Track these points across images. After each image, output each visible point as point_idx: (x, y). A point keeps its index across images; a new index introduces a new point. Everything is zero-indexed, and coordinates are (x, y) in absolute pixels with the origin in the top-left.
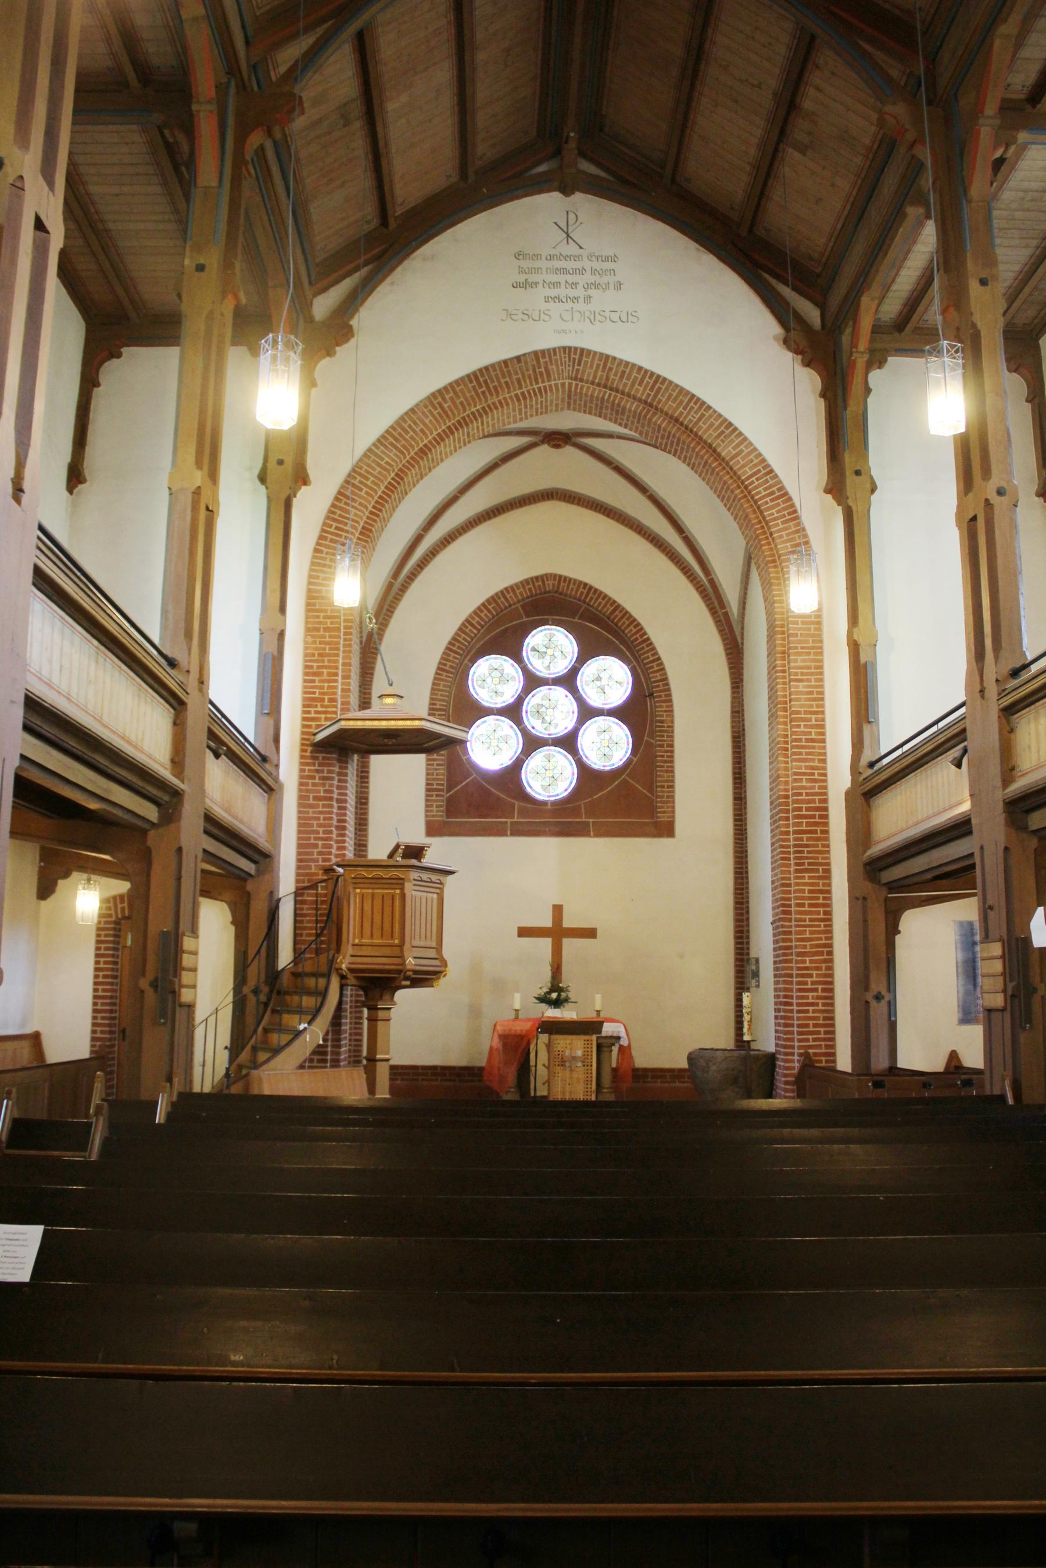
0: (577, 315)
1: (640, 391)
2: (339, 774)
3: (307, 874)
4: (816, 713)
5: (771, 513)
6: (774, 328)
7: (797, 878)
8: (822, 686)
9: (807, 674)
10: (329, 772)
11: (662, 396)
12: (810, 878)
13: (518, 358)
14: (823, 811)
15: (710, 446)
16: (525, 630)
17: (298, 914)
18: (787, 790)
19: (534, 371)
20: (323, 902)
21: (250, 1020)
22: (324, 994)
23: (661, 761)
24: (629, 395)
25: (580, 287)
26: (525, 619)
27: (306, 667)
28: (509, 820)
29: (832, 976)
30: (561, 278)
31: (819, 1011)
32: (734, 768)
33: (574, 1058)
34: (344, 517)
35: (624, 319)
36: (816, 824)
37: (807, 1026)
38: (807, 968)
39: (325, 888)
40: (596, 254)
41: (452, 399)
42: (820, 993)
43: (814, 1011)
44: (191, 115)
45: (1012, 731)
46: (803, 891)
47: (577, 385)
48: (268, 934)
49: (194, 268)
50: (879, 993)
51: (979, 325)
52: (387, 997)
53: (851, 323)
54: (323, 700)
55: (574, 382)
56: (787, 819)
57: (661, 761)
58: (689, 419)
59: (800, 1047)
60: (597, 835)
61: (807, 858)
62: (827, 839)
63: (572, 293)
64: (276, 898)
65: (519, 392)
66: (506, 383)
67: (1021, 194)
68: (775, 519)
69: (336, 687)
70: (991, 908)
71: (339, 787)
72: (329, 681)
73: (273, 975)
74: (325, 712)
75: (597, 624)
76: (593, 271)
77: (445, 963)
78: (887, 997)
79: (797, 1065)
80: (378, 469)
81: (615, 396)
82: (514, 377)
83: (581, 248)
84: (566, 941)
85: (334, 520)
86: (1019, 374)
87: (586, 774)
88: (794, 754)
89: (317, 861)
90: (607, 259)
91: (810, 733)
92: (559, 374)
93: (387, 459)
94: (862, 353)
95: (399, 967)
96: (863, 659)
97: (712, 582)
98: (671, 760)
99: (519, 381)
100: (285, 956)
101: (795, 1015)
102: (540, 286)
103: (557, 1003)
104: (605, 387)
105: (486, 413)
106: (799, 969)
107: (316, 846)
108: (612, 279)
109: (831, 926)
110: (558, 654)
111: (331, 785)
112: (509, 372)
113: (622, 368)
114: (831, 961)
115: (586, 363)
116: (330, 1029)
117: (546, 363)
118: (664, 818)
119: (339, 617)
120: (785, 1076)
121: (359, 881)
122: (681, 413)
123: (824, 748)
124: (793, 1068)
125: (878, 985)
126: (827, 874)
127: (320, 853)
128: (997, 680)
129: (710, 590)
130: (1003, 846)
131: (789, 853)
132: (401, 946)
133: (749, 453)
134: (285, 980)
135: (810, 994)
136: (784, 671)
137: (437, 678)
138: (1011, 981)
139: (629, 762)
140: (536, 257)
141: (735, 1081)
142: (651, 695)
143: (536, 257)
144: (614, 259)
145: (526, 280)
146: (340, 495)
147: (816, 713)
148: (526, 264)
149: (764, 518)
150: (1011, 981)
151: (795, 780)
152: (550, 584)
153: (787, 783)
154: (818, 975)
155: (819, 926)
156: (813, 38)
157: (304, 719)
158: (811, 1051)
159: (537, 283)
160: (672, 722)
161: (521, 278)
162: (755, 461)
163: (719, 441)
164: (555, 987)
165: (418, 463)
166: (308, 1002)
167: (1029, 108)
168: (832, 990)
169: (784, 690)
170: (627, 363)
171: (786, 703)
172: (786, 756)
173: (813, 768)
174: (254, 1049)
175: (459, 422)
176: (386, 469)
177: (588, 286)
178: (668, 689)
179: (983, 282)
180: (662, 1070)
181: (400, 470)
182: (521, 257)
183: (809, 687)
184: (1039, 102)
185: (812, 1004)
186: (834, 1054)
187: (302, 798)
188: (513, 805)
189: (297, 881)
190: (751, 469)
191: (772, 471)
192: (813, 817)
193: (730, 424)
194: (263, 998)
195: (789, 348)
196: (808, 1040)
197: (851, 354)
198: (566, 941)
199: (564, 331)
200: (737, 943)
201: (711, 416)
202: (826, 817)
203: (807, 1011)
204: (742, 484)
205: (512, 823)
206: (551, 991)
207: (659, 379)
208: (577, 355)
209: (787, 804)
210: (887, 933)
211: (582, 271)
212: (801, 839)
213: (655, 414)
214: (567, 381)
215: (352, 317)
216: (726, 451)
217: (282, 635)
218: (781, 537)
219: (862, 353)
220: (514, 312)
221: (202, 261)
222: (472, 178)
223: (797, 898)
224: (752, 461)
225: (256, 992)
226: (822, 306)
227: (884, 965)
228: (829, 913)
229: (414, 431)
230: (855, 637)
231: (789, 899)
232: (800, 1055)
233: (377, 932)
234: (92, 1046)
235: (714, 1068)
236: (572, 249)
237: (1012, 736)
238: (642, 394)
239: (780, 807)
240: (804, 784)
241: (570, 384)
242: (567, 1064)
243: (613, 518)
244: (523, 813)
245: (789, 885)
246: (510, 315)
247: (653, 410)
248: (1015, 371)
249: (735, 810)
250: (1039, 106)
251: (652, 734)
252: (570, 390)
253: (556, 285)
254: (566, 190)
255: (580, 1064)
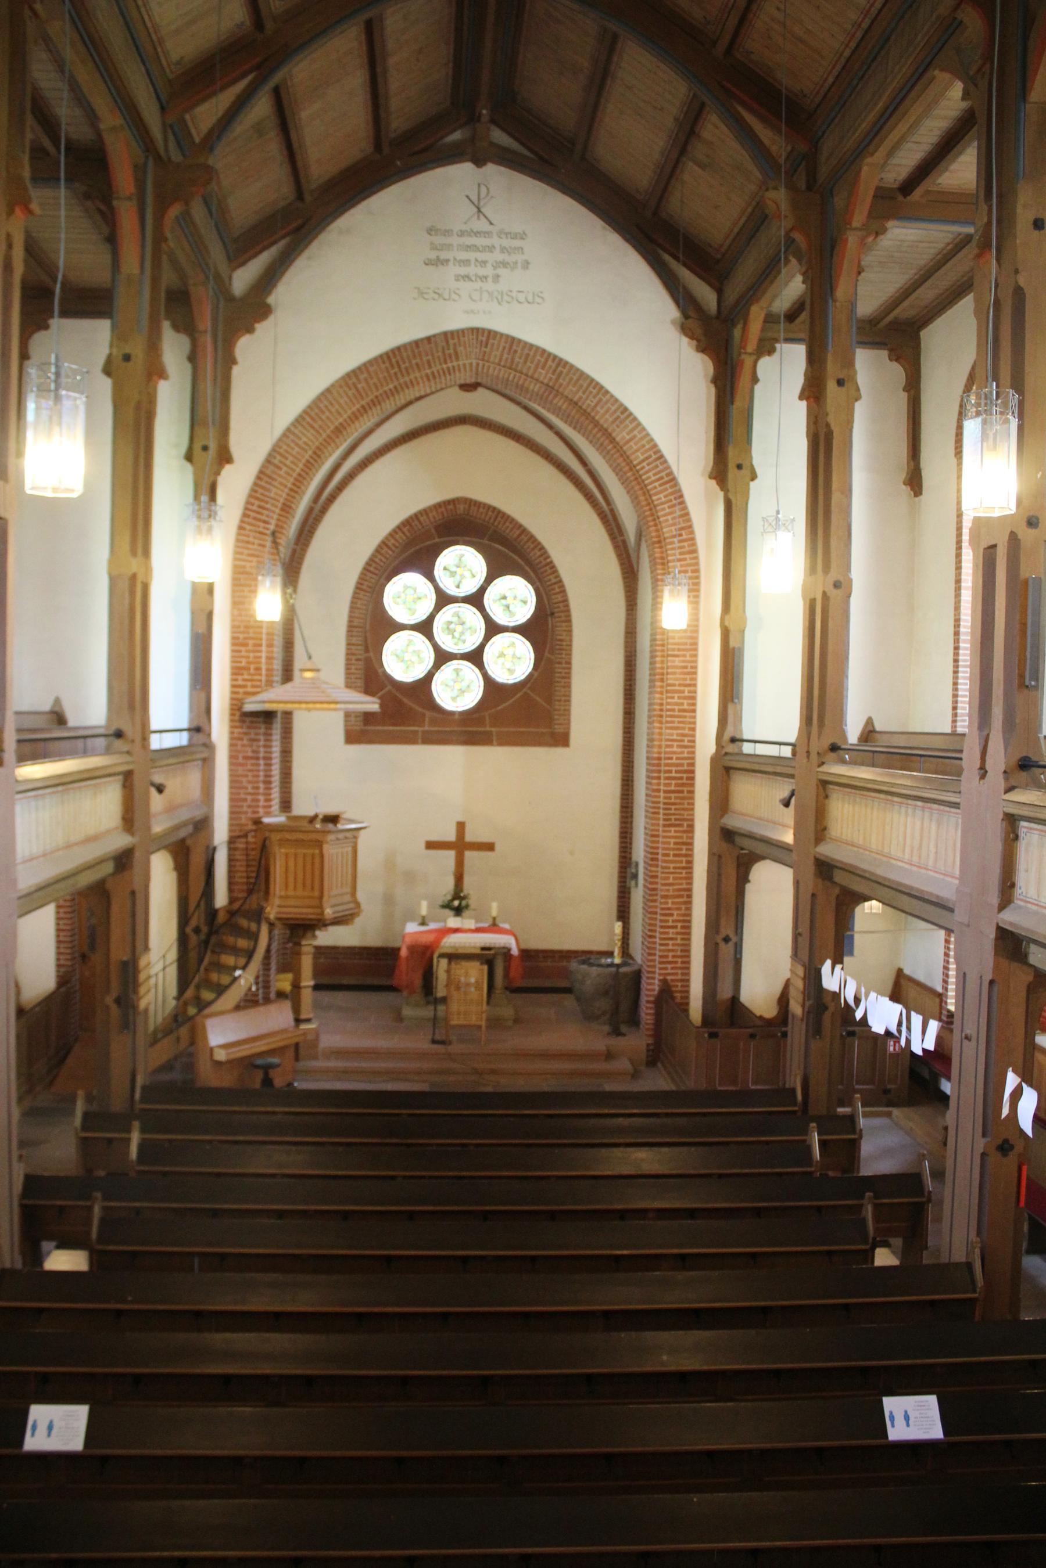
0: (485, 295)
1: (542, 374)
2: (265, 734)
3: (238, 825)
4: (689, 685)
5: (659, 498)
6: (672, 311)
7: (664, 831)
8: (696, 662)
9: (684, 650)
10: (257, 734)
11: (564, 380)
12: (676, 831)
13: (428, 339)
14: (691, 773)
15: (606, 430)
16: (435, 552)
17: (231, 860)
18: (660, 753)
19: (443, 352)
20: (252, 872)
21: (193, 955)
22: (255, 937)
23: (559, 677)
24: (532, 377)
25: (489, 265)
26: (437, 540)
27: (233, 638)
28: (420, 729)
29: (690, 915)
30: (472, 256)
31: (678, 945)
32: (625, 685)
33: (468, 985)
34: (266, 496)
35: (530, 299)
36: (683, 785)
37: (667, 957)
38: (669, 909)
39: (255, 837)
40: (506, 231)
41: (366, 380)
42: (679, 930)
43: (673, 945)
44: (112, 209)
45: (827, 797)
46: (669, 843)
47: (484, 365)
48: (203, 894)
49: (120, 358)
50: (727, 936)
51: (833, 426)
52: (309, 934)
53: (742, 322)
54: (249, 669)
55: (481, 363)
56: (659, 778)
57: (559, 677)
58: (589, 403)
59: (660, 974)
60: (500, 744)
61: (674, 814)
62: (692, 798)
63: (482, 271)
64: (211, 848)
65: (428, 371)
66: (417, 364)
67: (899, 243)
68: (663, 503)
69: (260, 657)
70: (800, 934)
71: (265, 746)
72: (253, 651)
73: (212, 913)
74: (252, 680)
75: (502, 544)
76: (503, 249)
77: (358, 905)
78: (734, 939)
79: (657, 988)
80: (297, 449)
81: (520, 377)
82: (425, 359)
83: (491, 224)
84: (468, 854)
85: (257, 499)
86: (900, 363)
87: (492, 688)
88: (667, 722)
89: (246, 813)
90: (515, 236)
91: (682, 704)
92: (467, 356)
93: (305, 439)
94: (750, 354)
95: (319, 917)
96: (733, 643)
97: (612, 511)
98: (568, 676)
99: (428, 362)
100: (221, 898)
101: (658, 947)
102: (451, 263)
103: (458, 911)
104: (510, 368)
105: (398, 392)
106: (663, 909)
107: (245, 800)
108: (519, 258)
109: (691, 873)
110: (468, 574)
111: (259, 746)
112: (420, 352)
113: (526, 351)
114: (690, 903)
115: (493, 345)
116: (261, 973)
117: (455, 345)
118: (559, 729)
119: (261, 627)
120: (647, 996)
121: (283, 842)
122: (581, 398)
123: (694, 717)
124: (653, 990)
125: (727, 930)
126: (691, 828)
127: (249, 806)
128: (818, 753)
129: (610, 517)
130: (811, 892)
131: (659, 808)
132: (321, 897)
133: (642, 439)
134: (221, 918)
135: (671, 931)
136: (663, 645)
137: (355, 597)
138: (809, 999)
139: (530, 675)
140: (447, 233)
141: (606, 993)
142: (552, 614)
143: (447, 233)
144: (522, 236)
145: (438, 257)
146: (261, 474)
147: (689, 685)
148: (439, 240)
149: (653, 501)
150: (809, 999)
151: (667, 746)
152: (461, 508)
153: (660, 746)
154: (678, 915)
155: (681, 873)
156: (703, 105)
157: (233, 686)
158: (669, 978)
159: (448, 261)
160: (571, 641)
161: (433, 255)
162: (647, 447)
163: (614, 426)
164: (458, 893)
165: (334, 441)
166: (242, 943)
167: (900, 198)
168: (689, 927)
169: (662, 662)
170: (531, 346)
171: (663, 674)
172: (661, 722)
173: (683, 735)
174: (198, 987)
175: (372, 401)
176: (303, 449)
177: (498, 264)
178: (567, 611)
179: (840, 383)
180: (553, 952)
181: (318, 448)
182: (433, 233)
183: (684, 661)
184: (909, 195)
185: (672, 939)
186: (688, 981)
187: (233, 758)
188: (424, 715)
189: (230, 831)
190: (642, 454)
191: (662, 456)
192: (681, 778)
193: (626, 409)
194: (203, 937)
195: (686, 335)
196: (666, 969)
197: (740, 354)
198: (468, 854)
199: (472, 312)
200: (621, 843)
201: (608, 401)
202: (693, 779)
203: (667, 945)
204: (632, 467)
205: (424, 732)
206: (454, 899)
207: (561, 363)
208: (484, 337)
209: (659, 765)
210: (737, 880)
211: (491, 249)
212: (670, 798)
213: (556, 396)
214: (474, 362)
215: (269, 293)
216: (621, 436)
217: (210, 616)
218: (667, 520)
219: (750, 354)
220: (425, 291)
221: (127, 351)
222: (386, 150)
223: (664, 849)
224: (644, 446)
225: (197, 930)
226: (720, 292)
227: (733, 912)
228: (690, 862)
229: (330, 412)
230: (727, 623)
231: (657, 848)
232: (660, 980)
233: (300, 885)
234: (58, 971)
235: (588, 982)
236: (481, 225)
237: (827, 801)
238: (545, 377)
239: (655, 764)
240: (675, 749)
241: (478, 364)
242: (462, 989)
243: (522, 444)
244: (433, 722)
245: (657, 836)
246: (421, 293)
247: (554, 392)
248: (896, 360)
249: (624, 723)
250: (908, 198)
251: (552, 651)
252: (477, 369)
253: (466, 263)
254: (479, 162)
255: (473, 989)
